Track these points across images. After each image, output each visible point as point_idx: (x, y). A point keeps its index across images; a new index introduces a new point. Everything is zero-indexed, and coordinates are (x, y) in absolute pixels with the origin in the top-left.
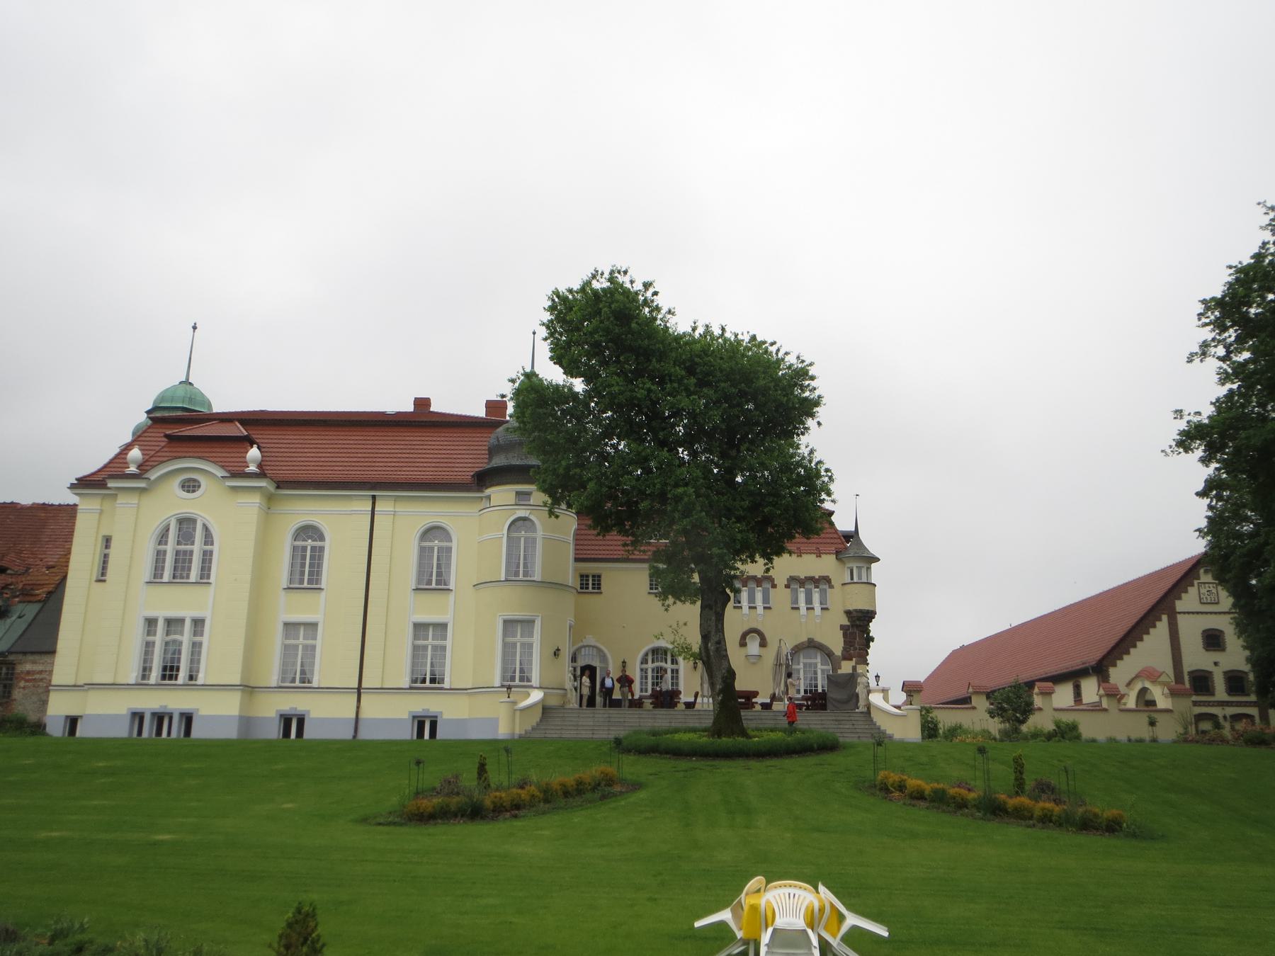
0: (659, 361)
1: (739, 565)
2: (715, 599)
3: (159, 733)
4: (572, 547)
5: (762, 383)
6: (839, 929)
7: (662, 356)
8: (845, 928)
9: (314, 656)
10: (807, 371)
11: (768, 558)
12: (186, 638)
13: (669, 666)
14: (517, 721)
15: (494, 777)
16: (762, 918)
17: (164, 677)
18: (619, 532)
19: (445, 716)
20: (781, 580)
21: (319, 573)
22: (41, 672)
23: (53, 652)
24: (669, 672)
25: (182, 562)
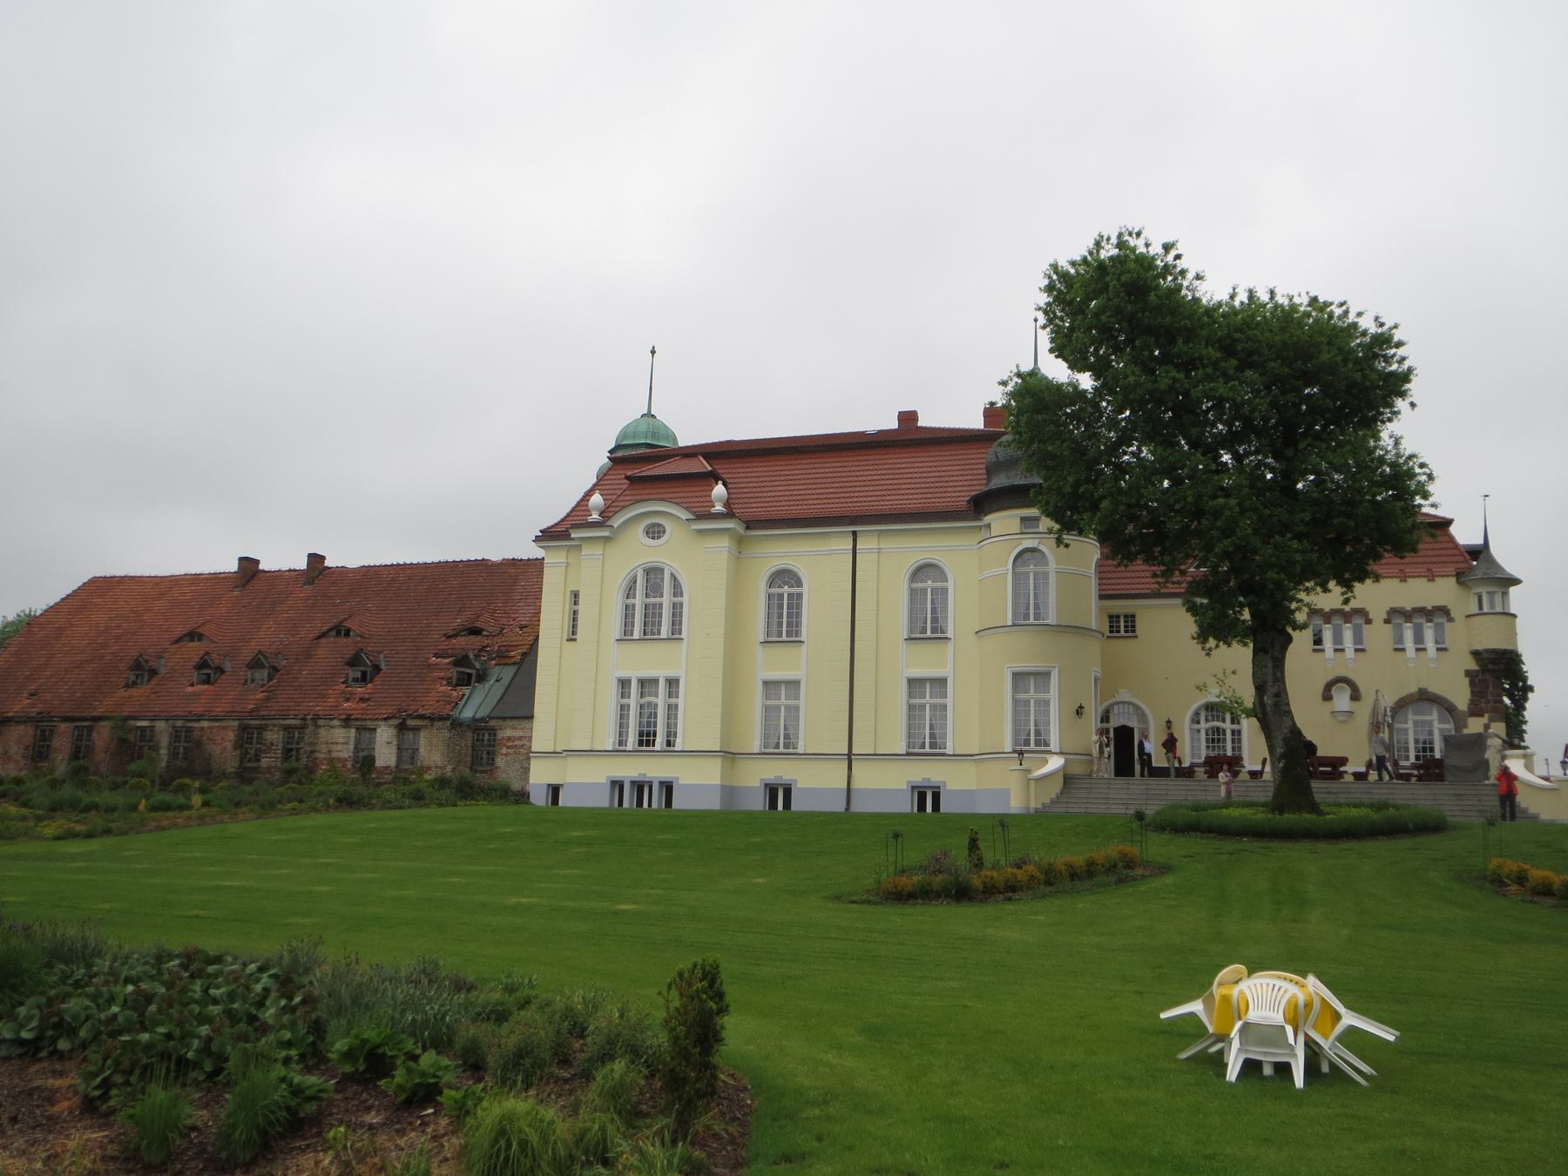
0: (1186, 342)
1: (1302, 595)
2: (1270, 639)
3: (640, 803)
4: (1094, 582)
5: (1325, 357)
6: (1334, 1026)
7: (1190, 334)
8: (1340, 1028)
9: (797, 719)
10: (1391, 337)
11: (1347, 585)
12: (661, 700)
13: (1228, 726)
14: (1032, 794)
15: (988, 856)
16: (1233, 1010)
17: (641, 743)
18: (1146, 561)
19: (948, 787)
20: (1378, 614)
21: (798, 624)
22: (520, 738)
23: (532, 717)
24: (1229, 733)
25: (652, 614)
